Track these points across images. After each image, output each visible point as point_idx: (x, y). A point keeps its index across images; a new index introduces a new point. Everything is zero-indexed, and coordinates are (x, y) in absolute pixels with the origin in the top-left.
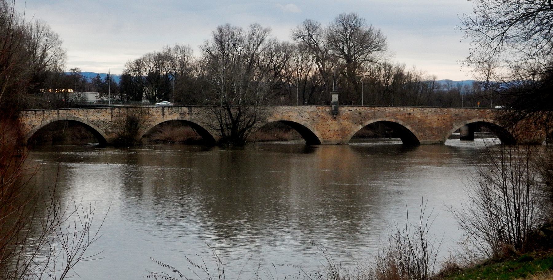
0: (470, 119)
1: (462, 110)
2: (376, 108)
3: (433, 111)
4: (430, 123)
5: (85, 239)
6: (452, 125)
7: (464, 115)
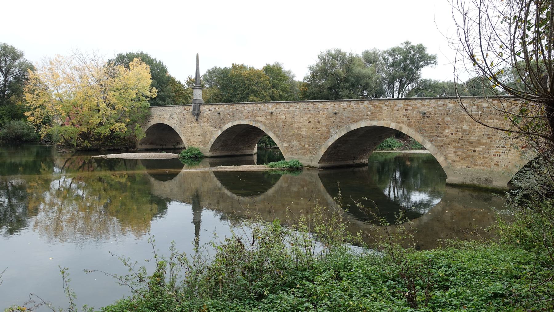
0: (356, 122)
1: (344, 104)
2: (235, 106)
3: (302, 109)
4: (298, 128)
5: (480, 62)
6: (328, 132)
7: (346, 114)
